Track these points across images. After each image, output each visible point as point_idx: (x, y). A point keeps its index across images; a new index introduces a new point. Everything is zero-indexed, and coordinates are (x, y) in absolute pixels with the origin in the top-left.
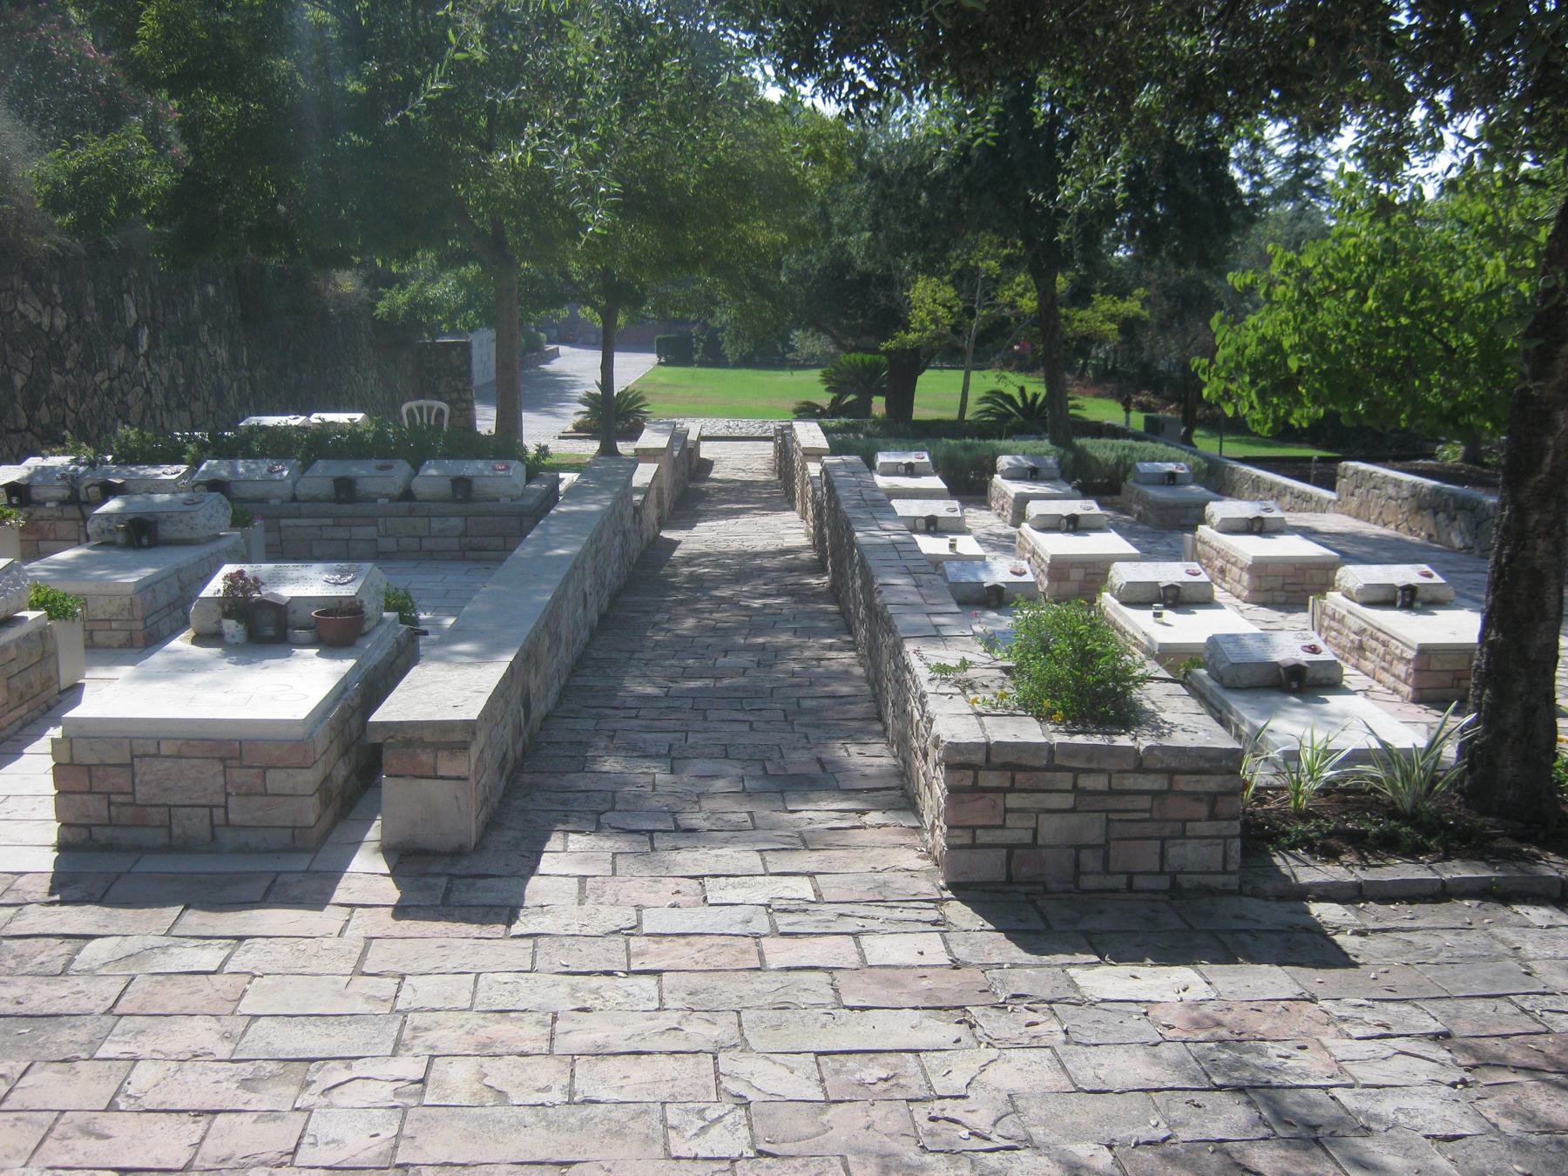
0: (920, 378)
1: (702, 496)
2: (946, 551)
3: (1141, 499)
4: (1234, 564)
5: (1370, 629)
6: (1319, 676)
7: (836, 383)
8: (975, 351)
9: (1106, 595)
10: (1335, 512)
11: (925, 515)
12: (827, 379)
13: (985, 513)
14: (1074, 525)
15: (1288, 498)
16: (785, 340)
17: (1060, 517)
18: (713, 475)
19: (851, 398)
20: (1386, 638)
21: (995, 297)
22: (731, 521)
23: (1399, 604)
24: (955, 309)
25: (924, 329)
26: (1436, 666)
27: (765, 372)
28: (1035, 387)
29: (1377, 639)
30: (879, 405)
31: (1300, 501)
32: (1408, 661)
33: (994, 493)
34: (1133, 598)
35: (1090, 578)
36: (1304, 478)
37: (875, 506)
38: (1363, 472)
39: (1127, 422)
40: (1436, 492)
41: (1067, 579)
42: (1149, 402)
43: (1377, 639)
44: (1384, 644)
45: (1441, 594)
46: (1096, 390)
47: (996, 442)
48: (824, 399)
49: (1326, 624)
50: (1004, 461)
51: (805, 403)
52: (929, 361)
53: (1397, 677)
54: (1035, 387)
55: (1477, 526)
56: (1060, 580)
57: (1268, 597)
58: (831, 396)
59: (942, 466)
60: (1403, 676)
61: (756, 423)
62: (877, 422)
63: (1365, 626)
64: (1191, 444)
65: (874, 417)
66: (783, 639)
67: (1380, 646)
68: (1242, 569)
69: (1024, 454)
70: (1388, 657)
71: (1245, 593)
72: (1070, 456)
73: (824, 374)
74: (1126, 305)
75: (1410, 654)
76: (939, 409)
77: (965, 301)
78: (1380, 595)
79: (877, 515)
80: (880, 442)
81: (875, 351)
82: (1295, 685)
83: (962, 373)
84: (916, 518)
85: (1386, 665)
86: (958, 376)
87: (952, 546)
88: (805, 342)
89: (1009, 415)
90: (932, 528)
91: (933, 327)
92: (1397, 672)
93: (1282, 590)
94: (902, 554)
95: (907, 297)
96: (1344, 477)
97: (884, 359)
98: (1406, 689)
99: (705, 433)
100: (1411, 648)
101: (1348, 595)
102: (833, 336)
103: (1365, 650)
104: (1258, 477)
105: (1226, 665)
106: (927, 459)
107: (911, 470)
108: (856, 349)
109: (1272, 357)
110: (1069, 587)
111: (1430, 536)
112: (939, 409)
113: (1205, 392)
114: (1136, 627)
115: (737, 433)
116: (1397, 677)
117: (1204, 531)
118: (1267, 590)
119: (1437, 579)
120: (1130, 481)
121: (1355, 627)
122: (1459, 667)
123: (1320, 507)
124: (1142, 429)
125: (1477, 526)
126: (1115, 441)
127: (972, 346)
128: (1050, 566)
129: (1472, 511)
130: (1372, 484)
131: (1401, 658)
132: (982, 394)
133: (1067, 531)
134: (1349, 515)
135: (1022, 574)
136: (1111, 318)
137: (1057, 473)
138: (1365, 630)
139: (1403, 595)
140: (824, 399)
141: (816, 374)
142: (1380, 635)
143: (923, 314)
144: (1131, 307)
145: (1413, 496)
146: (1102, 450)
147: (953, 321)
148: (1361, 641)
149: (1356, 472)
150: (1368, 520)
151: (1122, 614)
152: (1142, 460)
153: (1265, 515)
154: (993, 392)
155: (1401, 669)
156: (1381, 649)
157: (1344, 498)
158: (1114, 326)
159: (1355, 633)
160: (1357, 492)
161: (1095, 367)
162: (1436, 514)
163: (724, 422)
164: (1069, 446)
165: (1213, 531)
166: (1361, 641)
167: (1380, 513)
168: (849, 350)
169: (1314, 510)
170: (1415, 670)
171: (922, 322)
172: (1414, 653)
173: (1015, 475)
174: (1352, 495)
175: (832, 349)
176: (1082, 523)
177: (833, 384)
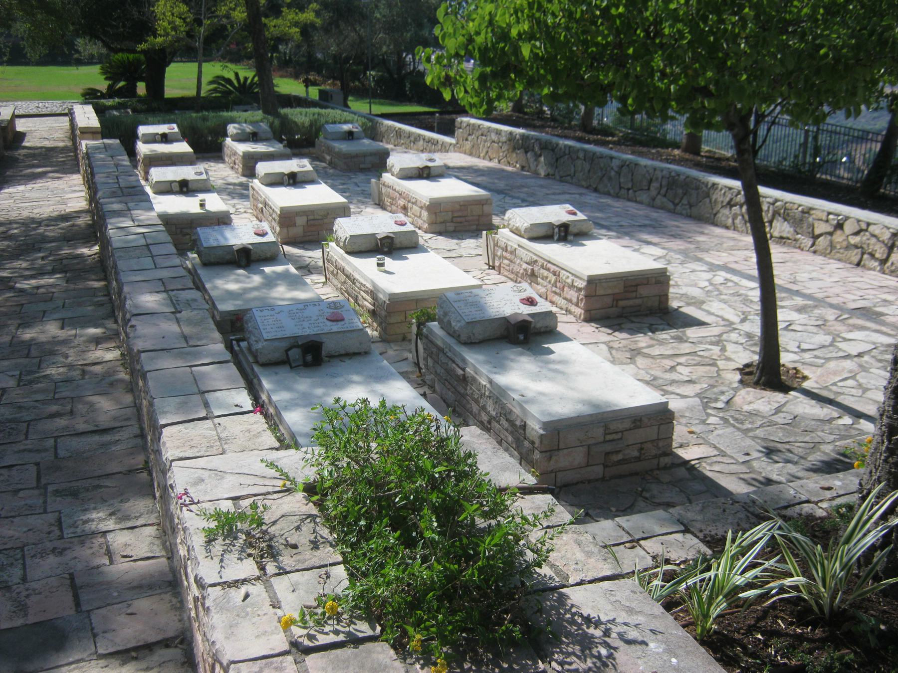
0: (167, 69)
1: (13, 162)
2: (196, 209)
3: (330, 150)
4: (415, 203)
5: (540, 261)
6: (539, 325)
7: (112, 74)
8: (204, 49)
9: (333, 244)
10: (455, 151)
11: (178, 179)
12: (104, 72)
13: (221, 165)
14: (293, 180)
15: (421, 142)
16: (71, 46)
17: (283, 174)
18: (25, 144)
19: (122, 84)
20: (557, 269)
21: (215, 11)
22: (29, 187)
23: (556, 238)
24: (188, 20)
25: (167, 34)
26: (600, 292)
27: (65, 68)
28: (247, 73)
29: (548, 270)
30: (141, 88)
31: (430, 144)
32: (580, 290)
33: (226, 151)
34: (356, 248)
35: (312, 222)
36: (430, 129)
37: (130, 195)
38: (474, 125)
39: (307, 92)
40: (523, 136)
41: (294, 225)
42: (316, 80)
43: (548, 270)
44: (554, 273)
45: (584, 228)
46: (281, 73)
47: (225, 114)
48: (102, 85)
49: (499, 253)
50: (232, 129)
51: (89, 89)
52: (172, 58)
53: (570, 301)
54: (247, 73)
55: (557, 160)
56: (288, 226)
57: (441, 228)
58: (108, 83)
59: (189, 134)
60: (575, 300)
61: (58, 103)
62: (141, 100)
63: (535, 258)
64: (346, 106)
65: (140, 97)
66: (52, 330)
67: (550, 275)
68: (421, 208)
69: (246, 122)
70: (558, 284)
71: (426, 226)
72: (277, 122)
73: (102, 68)
74: (304, 15)
75: (582, 284)
76: (183, 88)
77: (195, 14)
78: (542, 232)
79: (131, 205)
80: (142, 117)
81: (134, 51)
82: (521, 337)
83: (196, 65)
84: (172, 182)
85: (558, 291)
86: (194, 66)
87: (202, 205)
88: (85, 46)
89: (230, 92)
90: (185, 189)
91: (173, 33)
92: (568, 297)
93: (452, 221)
94: (158, 260)
95: (153, 11)
96: (460, 128)
97: (142, 57)
98: (579, 311)
99: (17, 112)
100: (581, 279)
101: (516, 232)
102: (103, 41)
103: (537, 277)
104: (400, 129)
105: (463, 323)
106: (176, 130)
107: (165, 138)
108: (121, 50)
109: (502, 45)
110: (297, 231)
111: (523, 168)
112: (183, 88)
113: (428, 80)
114: (364, 276)
115: (44, 111)
116: (570, 301)
117: (387, 177)
118: (441, 223)
119: (581, 216)
120: (321, 137)
121: (528, 259)
122: (617, 291)
123: (444, 148)
124: (317, 98)
125: (557, 160)
126: (308, 110)
127: (202, 46)
128: (280, 216)
129: (553, 150)
130: (480, 132)
131: (572, 286)
132: (210, 78)
133: (289, 185)
134: (465, 153)
135: (263, 235)
136: (296, 24)
137: (270, 135)
138: (536, 261)
139: (560, 231)
140: (102, 85)
141: (96, 69)
142: (549, 265)
143: (165, 24)
144: (308, 16)
145: (510, 140)
146: (300, 116)
147: (187, 28)
148: (533, 270)
149: (469, 125)
150: (479, 157)
151: (349, 263)
152: (327, 122)
153: (430, 164)
154: (218, 77)
155: (572, 294)
156: (553, 278)
157: (461, 142)
158: (297, 30)
159: (527, 263)
160: (470, 138)
161: (278, 59)
162: (526, 152)
163: (36, 104)
164: (277, 115)
165: (394, 178)
166: (533, 270)
167: (487, 152)
168: (116, 51)
169: (440, 151)
170: (586, 296)
171: (165, 29)
172: (585, 283)
173: (241, 138)
174: (467, 140)
175: (104, 51)
176: (299, 178)
177: (109, 75)
